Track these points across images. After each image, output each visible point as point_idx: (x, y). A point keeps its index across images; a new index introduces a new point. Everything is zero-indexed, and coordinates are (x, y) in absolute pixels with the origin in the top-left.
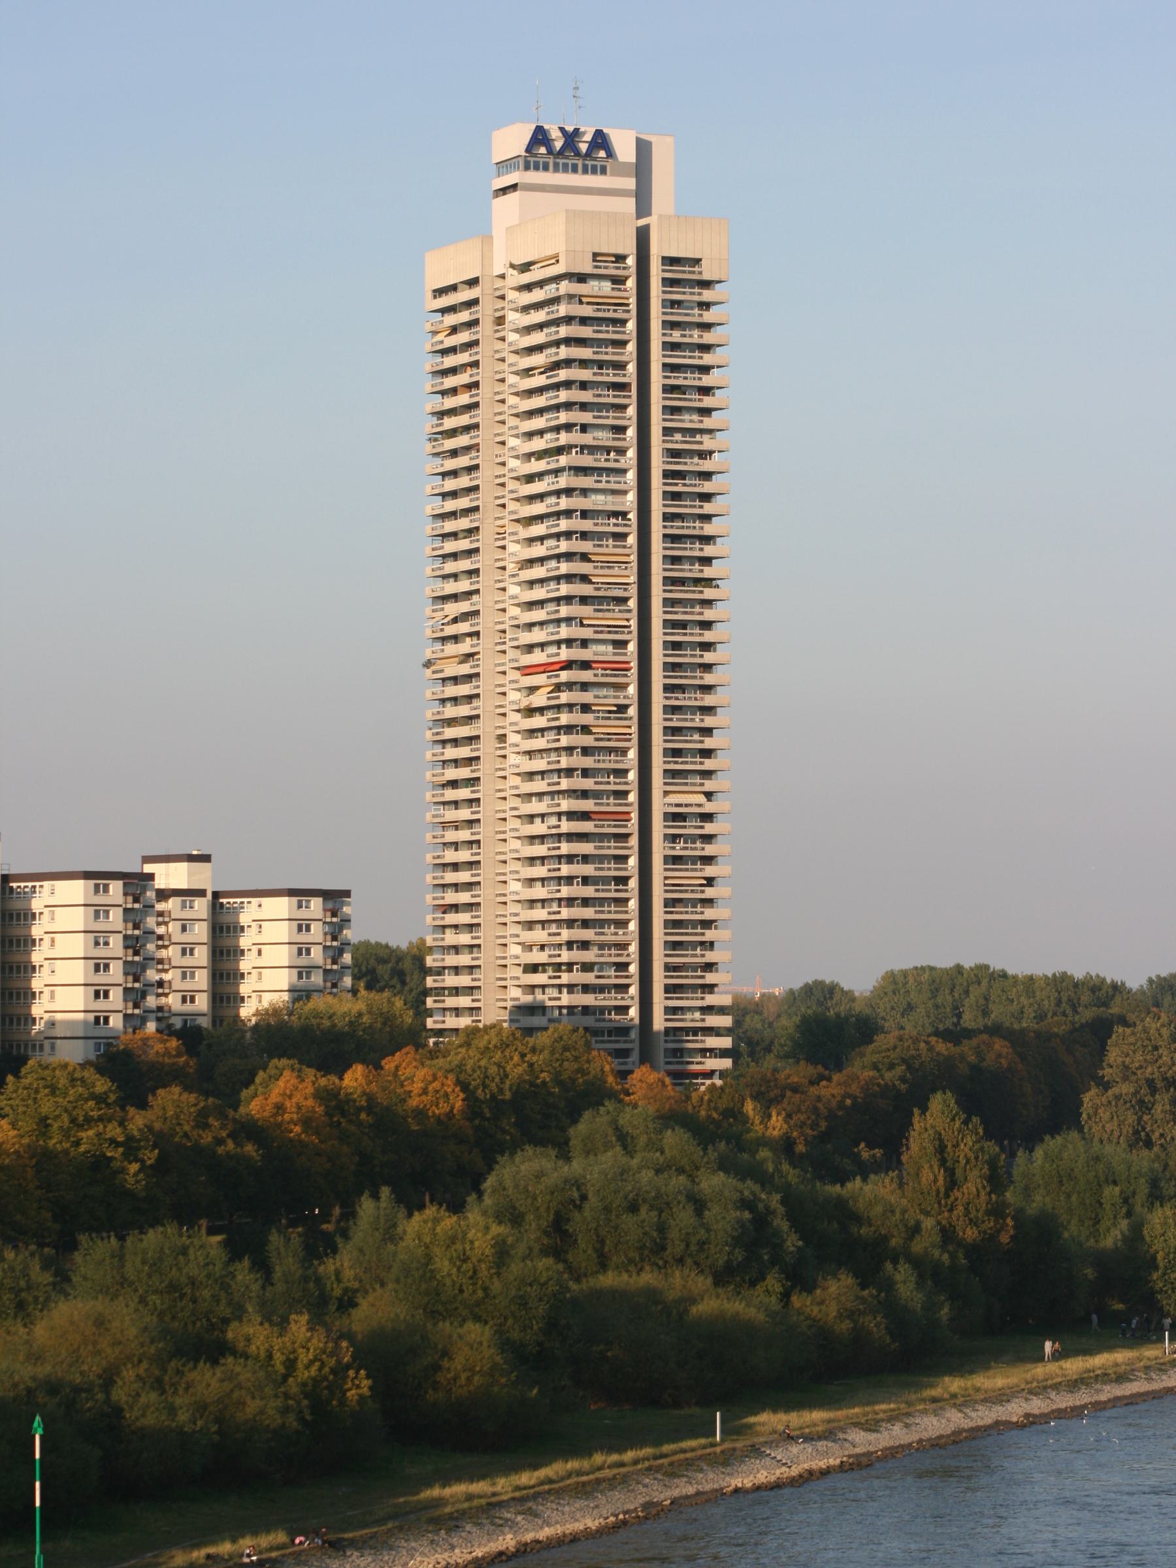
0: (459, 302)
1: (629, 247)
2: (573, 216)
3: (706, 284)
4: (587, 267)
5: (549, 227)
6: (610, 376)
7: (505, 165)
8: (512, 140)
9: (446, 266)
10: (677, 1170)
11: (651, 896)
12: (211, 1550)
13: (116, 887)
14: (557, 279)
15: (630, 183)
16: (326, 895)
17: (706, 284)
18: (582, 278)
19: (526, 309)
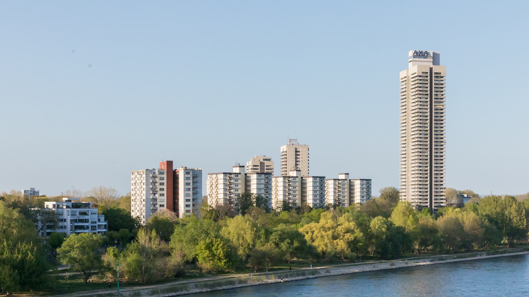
0: (405, 80)
1: (428, 71)
2: (418, 66)
3: (442, 77)
4: (421, 74)
5: (414, 68)
6: (425, 93)
7: (410, 57)
8: (411, 53)
9: (403, 74)
10: (179, 223)
11: (178, 194)
12: (280, 280)
13: (318, 179)
14: (416, 77)
15: (432, 60)
16: (367, 180)
17: (442, 77)
18: (420, 76)
19: (413, 81)
